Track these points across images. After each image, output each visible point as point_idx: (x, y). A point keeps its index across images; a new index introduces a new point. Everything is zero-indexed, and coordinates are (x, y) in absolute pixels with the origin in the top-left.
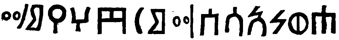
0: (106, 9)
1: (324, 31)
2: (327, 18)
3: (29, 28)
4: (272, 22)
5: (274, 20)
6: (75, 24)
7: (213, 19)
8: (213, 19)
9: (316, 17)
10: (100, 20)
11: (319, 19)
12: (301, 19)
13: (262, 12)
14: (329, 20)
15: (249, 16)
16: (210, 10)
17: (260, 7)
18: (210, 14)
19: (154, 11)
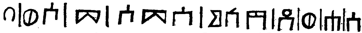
1: (338, 29)
3: (211, 25)
6: (130, 10)
10: (248, 16)
11: (329, 21)
13: (209, 27)
18: (232, 12)
19: (213, 12)
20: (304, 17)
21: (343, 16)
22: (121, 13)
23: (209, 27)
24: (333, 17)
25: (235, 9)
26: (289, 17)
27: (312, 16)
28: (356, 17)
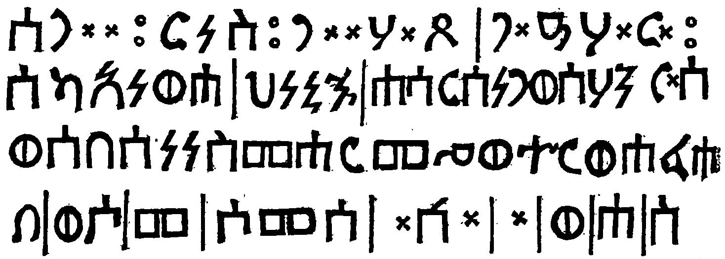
0: (254, 144)
1: (387, 102)
2: (210, 82)
4: (130, 87)
5: (133, 85)
7: (29, 85)
8: (29, 85)
9: (225, 219)
11: (609, 218)
12: (572, 216)
13: (76, 112)
14: (212, 85)
15: (117, 69)
16: (136, 129)
17: (637, 67)
20: (180, 97)
21: (584, 95)
22: (12, 80)
23: (76, 112)
24: (616, 210)
25: (444, 201)
26: (105, 72)
27: (174, 79)
28: (239, 210)
